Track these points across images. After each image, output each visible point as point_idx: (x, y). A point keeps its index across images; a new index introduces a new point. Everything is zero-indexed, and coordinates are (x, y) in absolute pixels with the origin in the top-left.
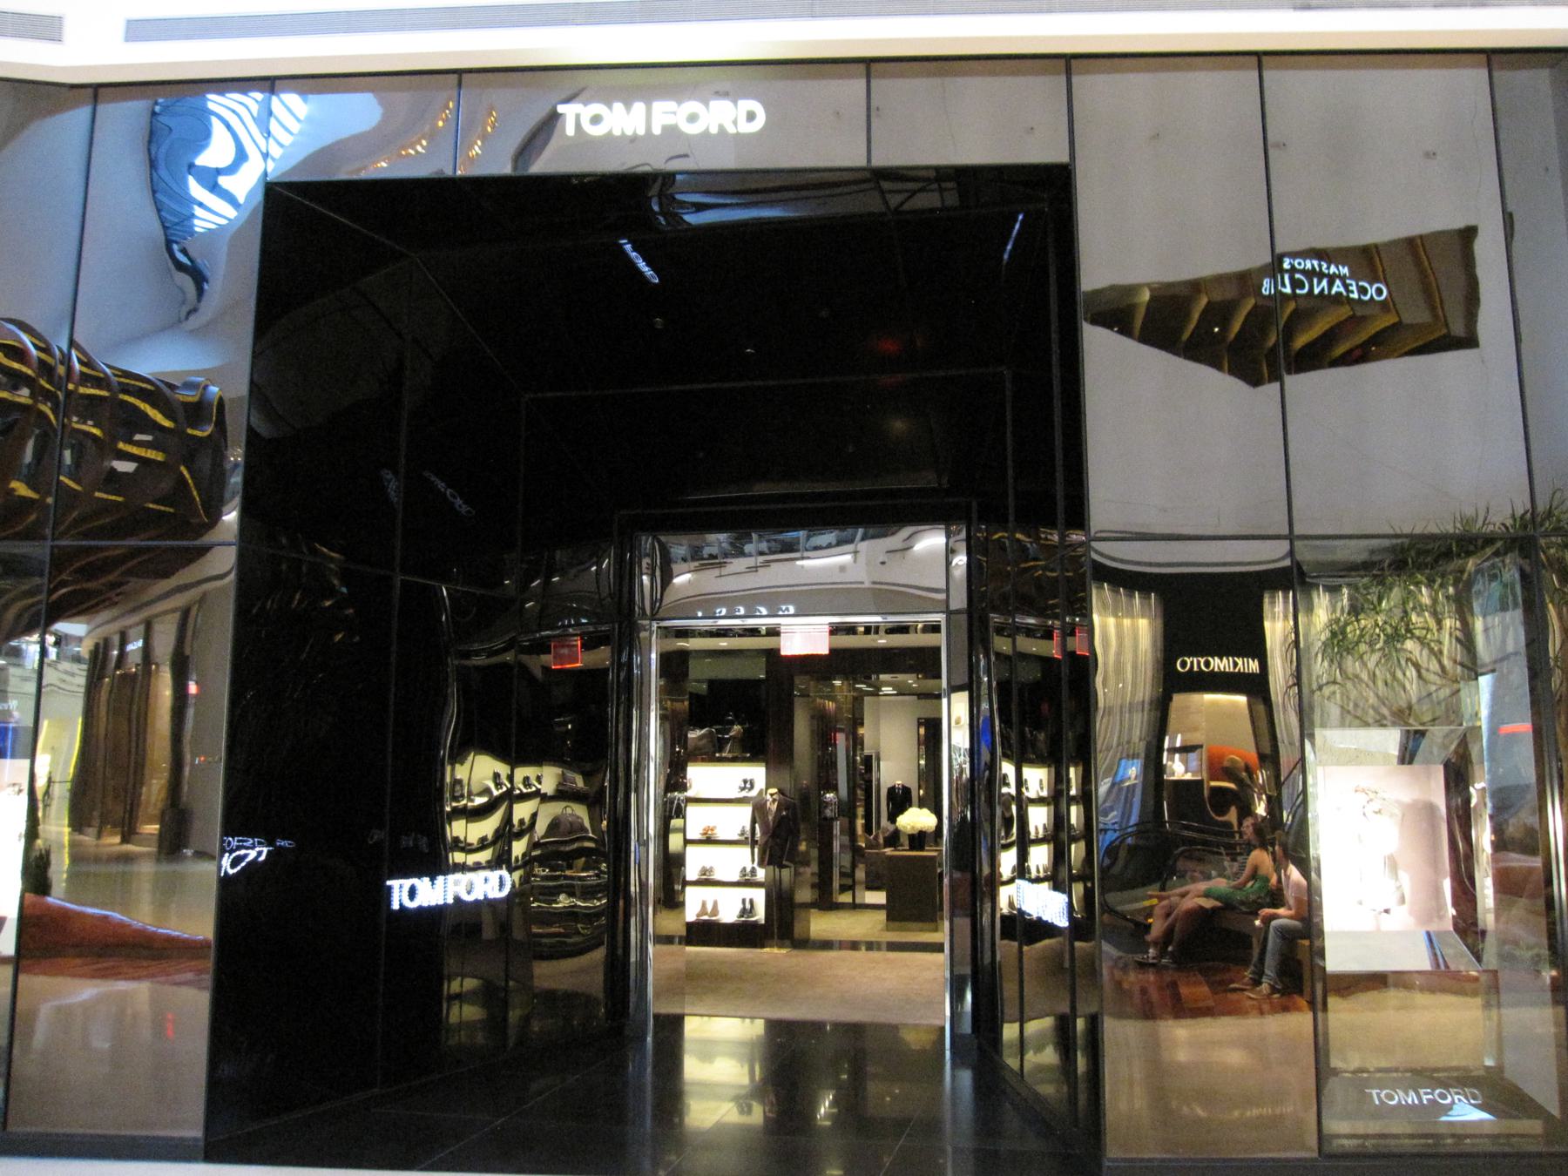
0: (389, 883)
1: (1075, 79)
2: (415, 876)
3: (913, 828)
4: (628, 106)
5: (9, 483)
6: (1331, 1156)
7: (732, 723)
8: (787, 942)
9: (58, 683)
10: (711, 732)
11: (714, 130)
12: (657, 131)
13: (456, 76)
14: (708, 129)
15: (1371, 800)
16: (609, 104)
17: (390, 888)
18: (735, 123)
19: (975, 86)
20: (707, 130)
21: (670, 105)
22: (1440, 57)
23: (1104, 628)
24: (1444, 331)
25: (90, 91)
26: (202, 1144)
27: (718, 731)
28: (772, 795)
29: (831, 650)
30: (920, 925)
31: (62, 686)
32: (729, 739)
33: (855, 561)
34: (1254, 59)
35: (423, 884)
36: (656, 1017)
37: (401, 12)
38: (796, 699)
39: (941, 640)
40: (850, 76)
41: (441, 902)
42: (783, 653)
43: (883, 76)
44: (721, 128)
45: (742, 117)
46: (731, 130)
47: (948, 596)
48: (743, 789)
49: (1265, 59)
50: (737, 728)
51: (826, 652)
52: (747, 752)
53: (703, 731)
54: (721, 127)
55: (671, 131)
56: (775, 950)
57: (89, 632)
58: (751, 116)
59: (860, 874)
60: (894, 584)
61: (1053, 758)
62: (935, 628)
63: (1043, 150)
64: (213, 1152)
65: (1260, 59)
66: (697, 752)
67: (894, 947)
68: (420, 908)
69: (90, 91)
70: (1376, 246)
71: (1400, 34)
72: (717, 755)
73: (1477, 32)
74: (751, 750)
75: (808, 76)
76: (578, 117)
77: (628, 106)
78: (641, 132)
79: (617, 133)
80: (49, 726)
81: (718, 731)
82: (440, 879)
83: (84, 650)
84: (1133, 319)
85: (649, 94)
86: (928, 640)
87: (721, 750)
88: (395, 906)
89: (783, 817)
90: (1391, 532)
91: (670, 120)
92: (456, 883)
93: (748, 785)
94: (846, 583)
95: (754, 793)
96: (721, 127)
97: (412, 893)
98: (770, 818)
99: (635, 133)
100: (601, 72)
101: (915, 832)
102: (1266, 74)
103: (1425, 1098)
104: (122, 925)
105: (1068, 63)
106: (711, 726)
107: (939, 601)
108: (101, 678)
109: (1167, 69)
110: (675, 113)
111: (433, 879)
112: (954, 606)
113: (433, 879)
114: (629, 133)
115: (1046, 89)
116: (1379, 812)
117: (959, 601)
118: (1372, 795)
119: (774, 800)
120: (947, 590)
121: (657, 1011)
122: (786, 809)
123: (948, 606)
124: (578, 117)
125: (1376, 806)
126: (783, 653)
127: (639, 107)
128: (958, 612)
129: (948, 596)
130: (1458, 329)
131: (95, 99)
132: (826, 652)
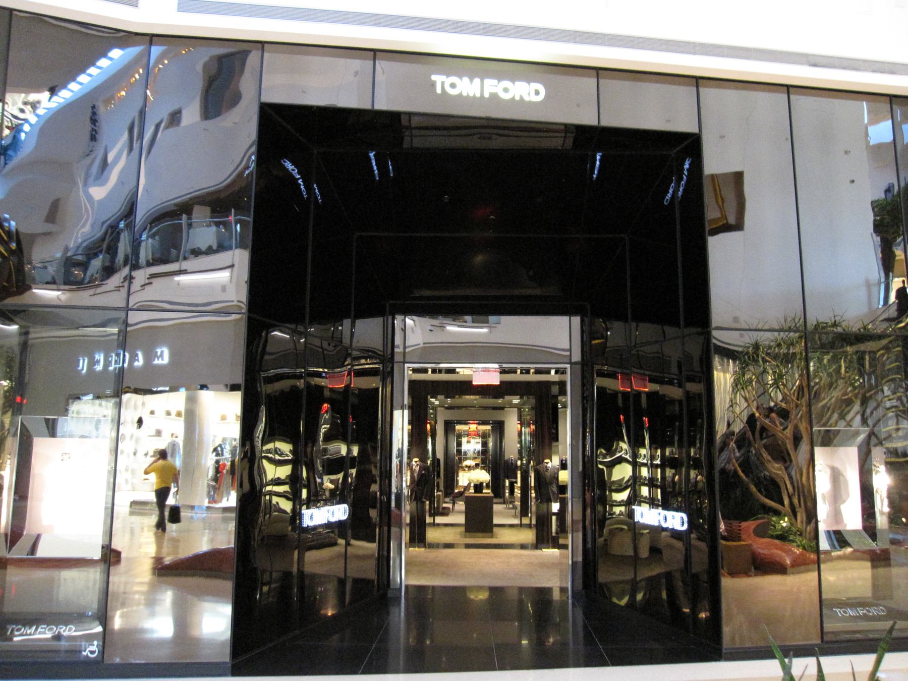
1: (701, 89)
3: (478, 481)
4: (471, 80)
6: (827, 642)
8: (422, 545)
12: (487, 95)
13: (372, 53)
14: (514, 97)
16: (460, 77)
18: (529, 94)
19: (653, 88)
20: (461, 93)
22: (766, 86)
23: (719, 378)
24: (725, 222)
25: (148, 38)
28: (416, 462)
29: (501, 382)
30: (484, 534)
33: (490, 333)
34: (695, 80)
37: (347, 13)
38: (559, 410)
39: (568, 378)
40: (589, 76)
42: (474, 383)
43: (605, 78)
45: (533, 93)
46: (527, 98)
47: (571, 353)
49: (700, 81)
51: (499, 383)
54: (521, 97)
55: (494, 96)
56: (417, 549)
60: (532, 346)
61: (291, 436)
63: (685, 125)
65: (788, 89)
67: (468, 546)
69: (148, 38)
70: (716, 175)
71: (879, 85)
73: (832, 81)
75: (567, 74)
76: (443, 83)
77: (471, 80)
78: (478, 95)
79: (465, 94)
84: (145, 172)
85: (484, 75)
89: (423, 474)
90: (747, 327)
91: (494, 90)
94: (433, 343)
96: (521, 97)
98: (416, 475)
99: (474, 96)
100: (455, 59)
101: (478, 483)
102: (792, 97)
103: (861, 612)
105: (698, 81)
107: (564, 356)
109: (746, 89)
112: (573, 360)
114: (471, 95)
115: (686, 93)
117: (577, 357)
119: (417, 465)
120: (570, 350)
121: (407, 583)
122: (425, 470)
123: (571, 360)
124: (443, 83)
126: (474, 383)
127: (477, 81)
128: (576, 363)
129: (571, 353)
130: (732, 220)
131: (151, 43)
132: (499, 383)
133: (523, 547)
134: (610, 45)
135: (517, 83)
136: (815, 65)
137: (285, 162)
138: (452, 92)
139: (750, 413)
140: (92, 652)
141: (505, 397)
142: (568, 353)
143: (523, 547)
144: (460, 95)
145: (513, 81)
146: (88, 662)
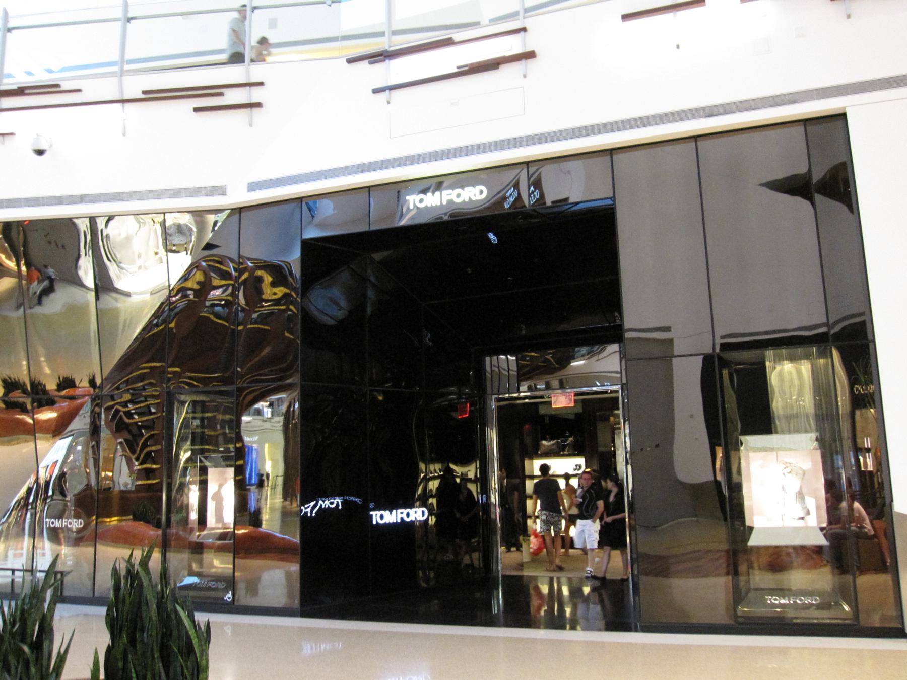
0: (371, 513)
2: (382, 510)
5: (252, 315)
7: (568, 437)
9: (271, 428)
10: (558, 442)
11: (467, 200)
12: (445, 203)
15: (787, 467)
17: (372, 515)
18: (475, 195)
21: (450, 191)
26: (299, 610)
27: (562, 441)
31: (273, 428)
32: (567, 444)
35: (386, 513)
36: (504, 576)
41: (395, 521)
44: (470, 199)
46: (474, 199)
48: (575, 470)
50: (571, 439)
52: (576, 451)
53: (554, 442)
55: (450, 202)
57: (288, 397)
58: (481, 192)
59: (825, 531)
62: (617, 392)
64: (305, 612)
65: (696, 138)
66: (823, 441)
68: (385, 524)
72: (562, 453)
74: (577, 451)
76: (414, 200)
79: (429, 205)
80: (269, 447)
81: (562, 441)
82: (394, 511)
83: (284, 408)
86: (614, 395)
87: (563, 450)
88: (374, 523)
91: (450, 198)
92: (402, 513)
93: (578, 468)
95: (580, 472)
97: (382, 517)
104: (289, 541)
106: (558, 439)
108: (288, 424)
110: (451, 194)
111: (391, 512)
113: (391, 512)
116: (790, 472)
118: (788, 465)
120: (621, 373)
121: (504, 573)
124: (414, 200)
125: (788, 470)
129: (621, 375)
133: (636, 535)
134: (528, 145)
135: (467, 189)
136: (711, 116)
137: (494, 240)
138: (421, 206)
139: (56, 399)
140: (229, 598)
141: (270, 410)
142: (619, 375)
143: (636, 535)
144: (426, 207)
145: (462, 187)
146: (227, 604)
